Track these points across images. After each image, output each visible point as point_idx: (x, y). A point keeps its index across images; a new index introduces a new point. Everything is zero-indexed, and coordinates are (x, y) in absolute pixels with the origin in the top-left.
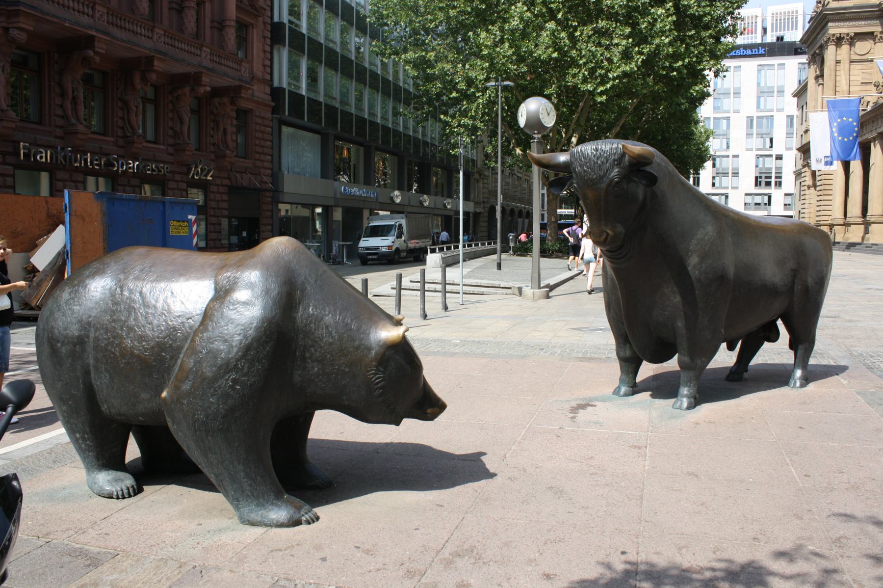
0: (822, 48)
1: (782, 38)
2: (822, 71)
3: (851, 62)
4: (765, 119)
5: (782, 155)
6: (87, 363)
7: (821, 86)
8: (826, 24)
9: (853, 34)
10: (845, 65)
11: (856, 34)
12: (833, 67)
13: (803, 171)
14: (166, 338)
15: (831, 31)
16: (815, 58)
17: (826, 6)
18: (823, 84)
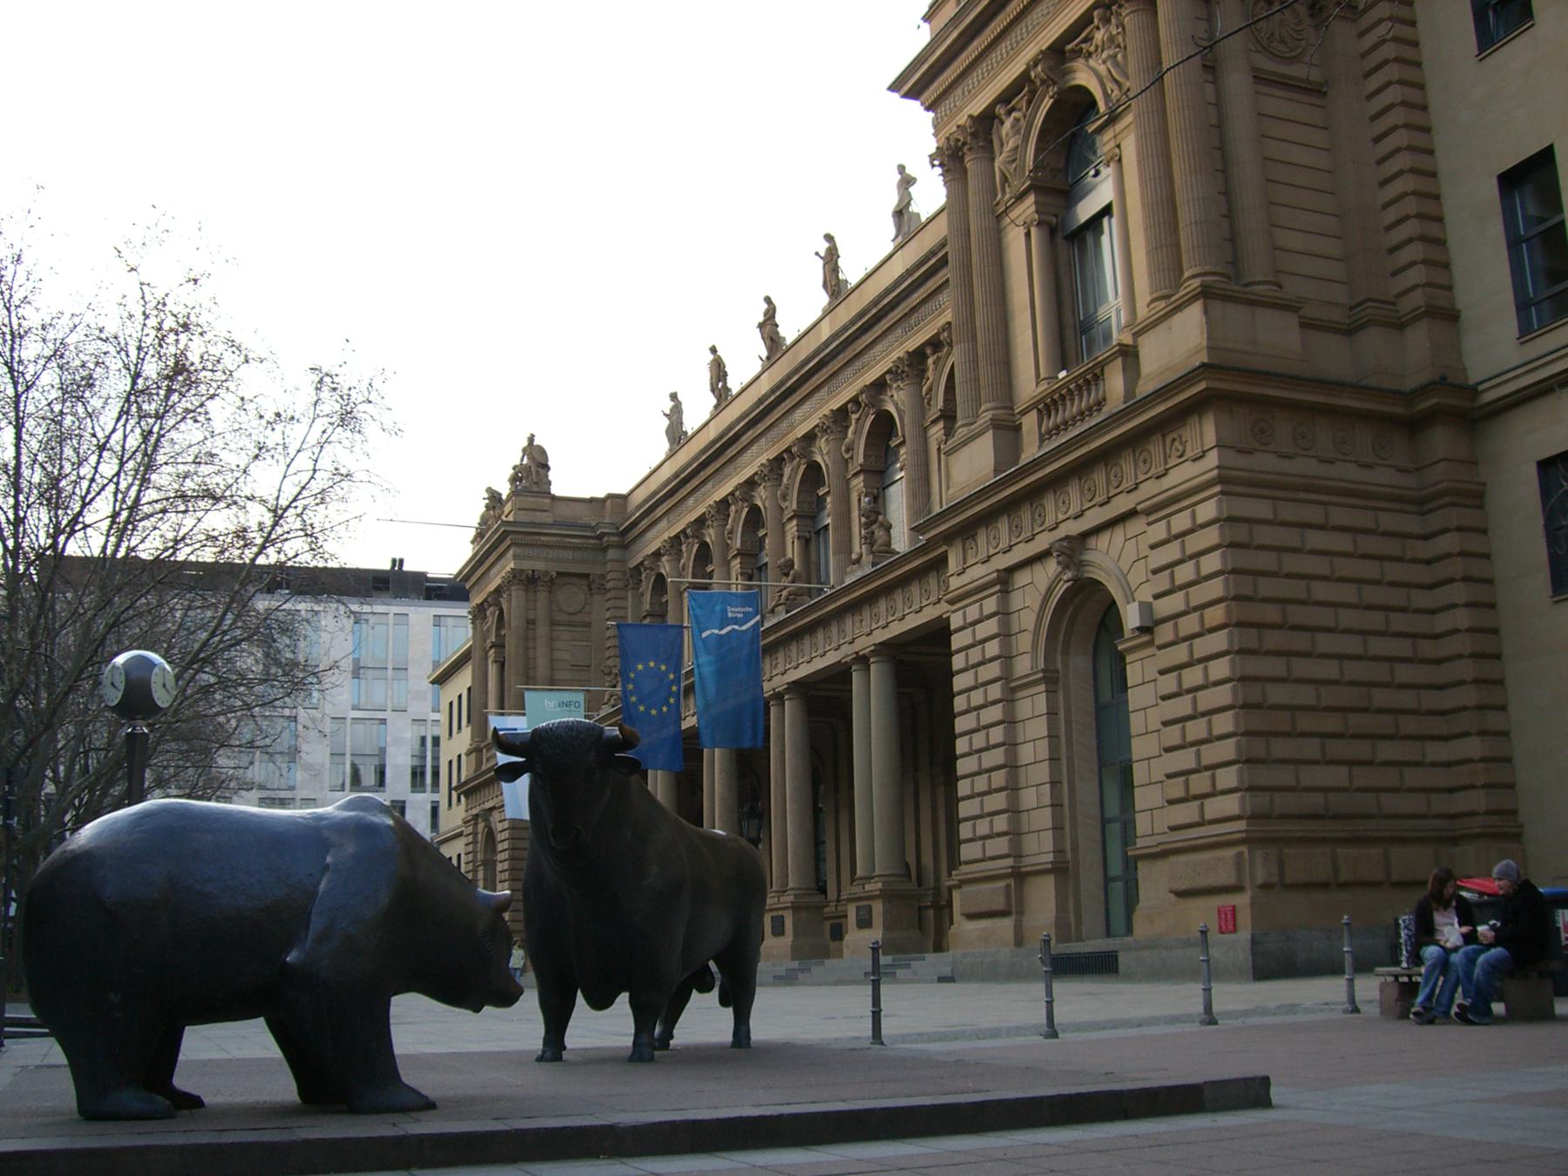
1: (401, 561)
5: (404, 802)
9: (555, 575)
10: (542, 630)
11: (559, 574)
16: (485, 610)
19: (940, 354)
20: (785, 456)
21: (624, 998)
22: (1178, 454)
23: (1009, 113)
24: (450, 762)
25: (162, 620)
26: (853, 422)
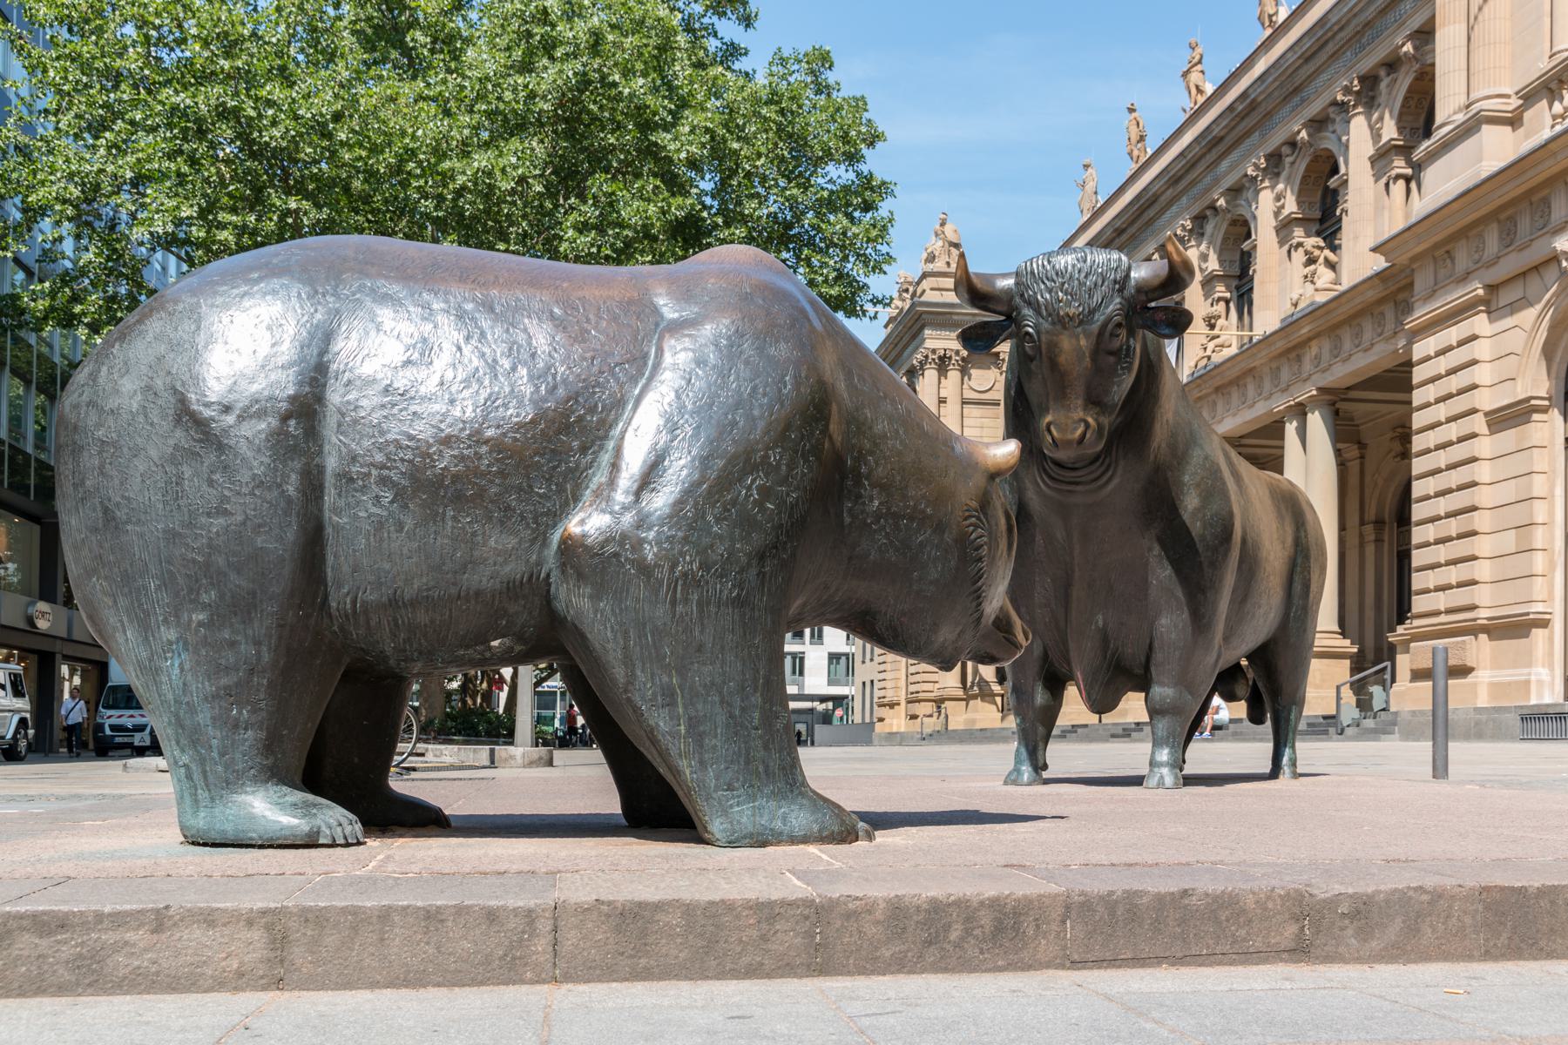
3: (964, 402)
6: (318, 466)
14: (568, 401)
15: (929, 344)
19: (1394, 75)
20: (1208, 213)
26: (1287, 166)
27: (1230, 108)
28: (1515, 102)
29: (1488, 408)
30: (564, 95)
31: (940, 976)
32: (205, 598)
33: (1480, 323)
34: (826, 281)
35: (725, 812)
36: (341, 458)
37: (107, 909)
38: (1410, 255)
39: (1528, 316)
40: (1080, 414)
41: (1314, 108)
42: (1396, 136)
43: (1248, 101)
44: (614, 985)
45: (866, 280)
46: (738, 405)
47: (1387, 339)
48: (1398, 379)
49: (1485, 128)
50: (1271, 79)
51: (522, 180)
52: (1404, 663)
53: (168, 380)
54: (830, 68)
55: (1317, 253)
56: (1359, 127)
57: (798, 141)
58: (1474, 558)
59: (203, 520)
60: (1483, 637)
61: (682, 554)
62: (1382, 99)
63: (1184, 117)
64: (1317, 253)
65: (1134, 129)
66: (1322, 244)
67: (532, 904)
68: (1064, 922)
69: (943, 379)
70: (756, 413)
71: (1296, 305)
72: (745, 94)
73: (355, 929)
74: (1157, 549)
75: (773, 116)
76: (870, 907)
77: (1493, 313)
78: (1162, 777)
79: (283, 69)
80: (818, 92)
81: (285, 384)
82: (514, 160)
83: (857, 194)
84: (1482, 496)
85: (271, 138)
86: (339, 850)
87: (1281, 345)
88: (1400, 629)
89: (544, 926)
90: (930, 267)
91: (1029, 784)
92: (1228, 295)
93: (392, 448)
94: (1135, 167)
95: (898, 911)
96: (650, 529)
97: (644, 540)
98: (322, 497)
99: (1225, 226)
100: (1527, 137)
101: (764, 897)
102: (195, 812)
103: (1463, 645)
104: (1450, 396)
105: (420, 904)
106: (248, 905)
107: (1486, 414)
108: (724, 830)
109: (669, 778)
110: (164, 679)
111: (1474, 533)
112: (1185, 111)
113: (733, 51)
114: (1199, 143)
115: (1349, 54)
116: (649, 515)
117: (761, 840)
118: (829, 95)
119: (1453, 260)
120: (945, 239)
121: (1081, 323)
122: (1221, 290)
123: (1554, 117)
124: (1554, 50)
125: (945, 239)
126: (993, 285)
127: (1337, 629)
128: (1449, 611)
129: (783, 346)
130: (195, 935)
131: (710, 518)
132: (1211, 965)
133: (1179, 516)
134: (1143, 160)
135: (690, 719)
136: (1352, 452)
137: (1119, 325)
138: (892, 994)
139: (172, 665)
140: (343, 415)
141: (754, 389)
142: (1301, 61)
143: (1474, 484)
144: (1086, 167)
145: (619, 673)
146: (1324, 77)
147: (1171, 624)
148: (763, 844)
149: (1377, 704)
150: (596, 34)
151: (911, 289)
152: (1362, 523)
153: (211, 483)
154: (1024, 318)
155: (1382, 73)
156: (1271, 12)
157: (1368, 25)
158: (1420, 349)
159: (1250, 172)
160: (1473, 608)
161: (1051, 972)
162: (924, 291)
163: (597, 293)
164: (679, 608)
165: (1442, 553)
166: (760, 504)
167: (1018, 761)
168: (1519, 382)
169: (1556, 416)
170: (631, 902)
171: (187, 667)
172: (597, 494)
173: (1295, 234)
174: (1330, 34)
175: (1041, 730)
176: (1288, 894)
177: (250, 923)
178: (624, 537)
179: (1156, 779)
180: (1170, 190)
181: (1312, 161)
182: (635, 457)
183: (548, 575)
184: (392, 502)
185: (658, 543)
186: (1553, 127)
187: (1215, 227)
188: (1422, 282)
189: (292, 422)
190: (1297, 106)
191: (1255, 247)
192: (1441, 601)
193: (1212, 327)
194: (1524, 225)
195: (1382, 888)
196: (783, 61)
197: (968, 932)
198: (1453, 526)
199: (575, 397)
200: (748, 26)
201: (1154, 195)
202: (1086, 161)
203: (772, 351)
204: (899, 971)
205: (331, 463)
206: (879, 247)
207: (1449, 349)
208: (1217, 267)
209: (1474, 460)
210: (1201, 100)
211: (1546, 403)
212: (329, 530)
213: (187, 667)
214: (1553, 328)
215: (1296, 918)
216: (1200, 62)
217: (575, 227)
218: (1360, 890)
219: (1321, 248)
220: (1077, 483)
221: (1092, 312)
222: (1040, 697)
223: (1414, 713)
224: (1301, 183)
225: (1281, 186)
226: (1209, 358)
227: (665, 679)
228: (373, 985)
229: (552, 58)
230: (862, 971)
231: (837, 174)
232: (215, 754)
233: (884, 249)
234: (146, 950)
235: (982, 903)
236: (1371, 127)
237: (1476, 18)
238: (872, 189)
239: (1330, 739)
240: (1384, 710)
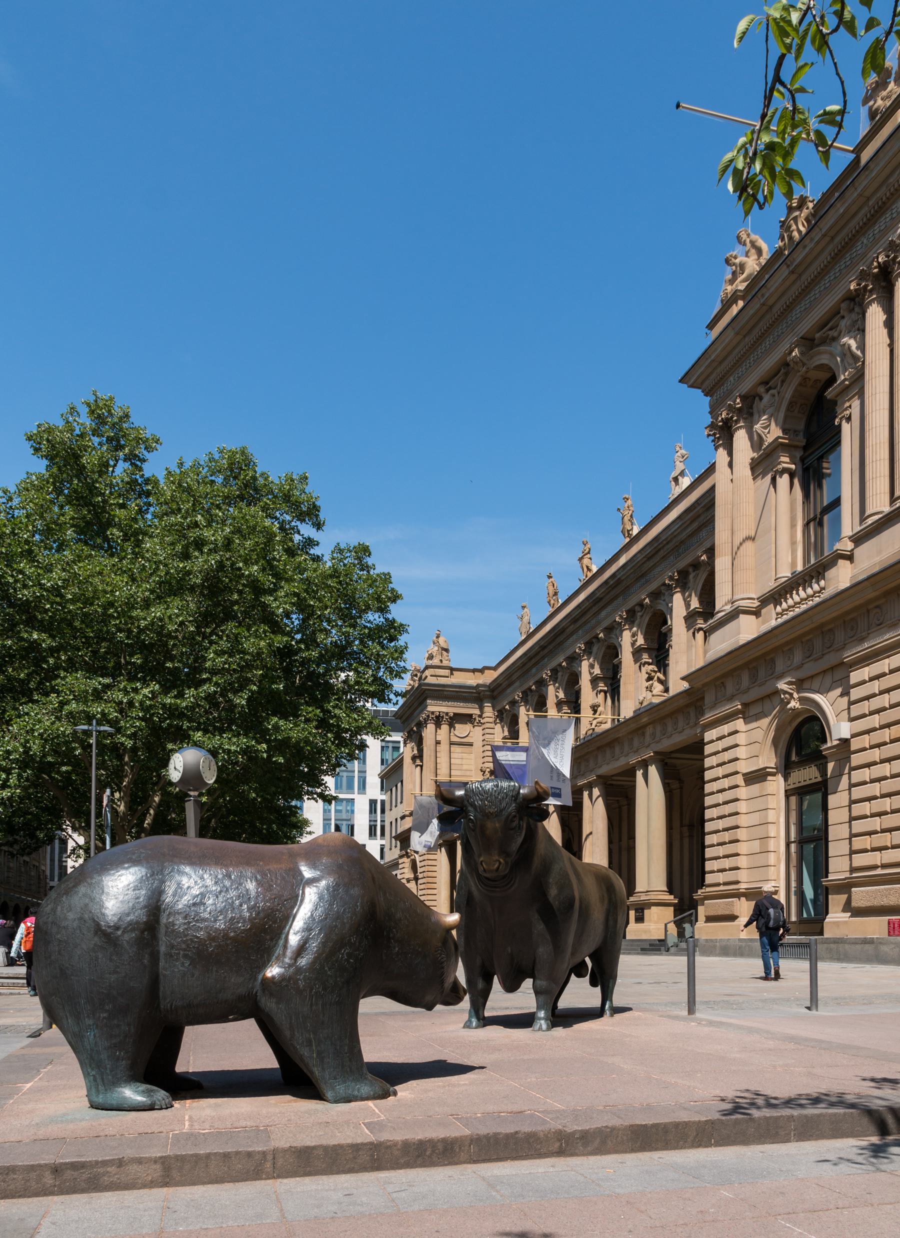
0: (421, 725)
2: (421, 750)
3: (452, 744)
4: (345, 802)
7: (419, 767)
8: (425, 699)
10: (444, 748)
11: (455, 714)
12: (433, 748)
13: (401, 861)
15: (430, 708)
17: (424, 679)
18: (422, 766)
19: (698, 572)
20: (594, 640)
21: (528, 983)
22: (878, 622)
23: (767, 391)
24: (391, 823)
25: (236, 751)
27: (606, 582)
28: (756, 603)
29: (745, 771)
30: (208, 574)
31: (423, 1169)
32: (107, 1007)
33: (739, 724)
34: (366, 682)
35: (333, 1089)
36: (167, 946)
37: (100, 1159)
38: (702, 683)
39: (765, 722)
40: (497, 858)
41: (653, 586)
42: (698, 606)
43: (616, 579)
44: (297, 1179)
45: (392, 682)
46: (337, 918)
47: (692, 727)
48: (697, 747)
49: (741, 616)
50: (629, 568)
51: (182, 623)
52: (701, 910)
53: (91, 915)
54: (369, 556)
55: (653, 674)
56: (678, 600)
57: (351, 601)
58: (737, 855)
59: (107, 976)
60: (743, 899)
61: (315, 985)
62: (691, 584)
63: (579, 584)
64: (653, 674)
65: (551, 588)
66: (656, 669)
67: (265, 1149)
68: (470, 1146)
69: (438, 730)
70: (345, 921)
71: (641, 703)
72: (318, 573)
73: (196, 1162)
74: (536, 916)
75: (335, 585)
76: (395, 1144)
77: (747, 720)
78: (541, 1025)
79: (30, 552)
80: (362, 570)
81: (140, 915)
82: (176, 611)
83: (386, 632)
84: (742, 820)
85: (23, 595)
86: (164, 1110)
87: (633, 726)
88: (700, 892)
89: (270, 1157)
90: (430, 662)
91: (476, 1028)
92: (606, 688)
93: (189, 942)
94: (552, 610)
95: (406, 1145)
96: (301, 974)
97: (299, 979)
98: (158, 964)
99: (603, 649)
100: (763, 623)
101: (355, 1142)
102: (97, 1096)
103: (732, 904)
104: (724, 763)
105: (221, 1151)
106: (154, 1155)
107: (744, 775)
108: (333, 1096)
109: (309, 1074)
110: (86, 1040)
111: (737, 841)
112: (580, 580)
113: (310, 543)
114: (589, 601)
115: (672, 557)
116: (301, 968)
117: (348, 1100)
118: (368, 572)
119: (725, 687)
120: (439, 646)
121: (496, 816)
122: (602, 686)
123: (778, 614)
124: (778, 576)
125: (439, 646)
126: (454, 794)
127: (665, 889)
128: (725, 884)
129: (356, 889)
130: (134, 1168)
131: (326, 968)
132: (526, 1159)
133: (548, 899)
134: (556, 606)
135: (318, 1051)
136: (675, 785)
137: (515, 816)
138: (404, 1180)
139: (90, 1034)
140: (168, 928)
141: (344, 910)
142: (645, 559)
143: (737, 813)
144: (523, 607)
145: (288, 1033)
146: (659, 569)
147: (543, 951)
148: (350, 1101)
149: (688, 934)
150: (228, 539)
151: (419, 675)
152: (682, 826)
153: (111, 960)
154: (469, 811)
155: (691, 570)
156: (629, 529)
157: (682, 542)
158: (709, 735)
159: (617, 619)
160: (737, 882)
161: (465, 1165)
162: (426, 677)
163: (275, 867)
164: (314, 1008)
165: (721, 851)
166: (347, 960)
167: (470, 1016)
168: (761, 758)
169: (780, 778)
170: (304, 1147)
171: (97, 1035)
172: (278, 958)
173: (644, 657)
174: (661, 546)
175: (481, 1000)
176: (556, 1131)
177: (155, 1162)
178: (290, 978)
179: (538, 1026)
180: (572, 626)
181: (652, 616)
182: (294, 940)
183: (256, 993)
184: (189, 965)
185: (305, 981)
186: (776, 619)
187: (598, 649)
188: (709, 699)
189: (146, 933)
190: (644, 584)
191: (621, 662)
192: (721, 878)
193: (595, 712)
194: (762, 673)
195: (592, 1127)
196: (341, 551)
197: (433, 1151)
198: (726, 836)
199: (267, 916)
200: (318, 529)
201: (563, 628)
202: (524, 604)
203: (352, 892)
204: (407, 1168)
205: (163, 949)
206: (399, 663)
207: (723, 737)
208: (599, 672)
209: (737, 800)
210: (590, 575)
211: (775, 770)
212: (161, 977)
213: (97, 1035)
214: (777, 730)
215: (559, 1140)
216: (589, 553)
217: (215, 652)
218: (583, 1128)
219: (655, 672)
220: (496, 887)
221: (501, 811)
222: (480, 985)
223: (706, 940)
224: (646, 628)
225: (635, 629)
226: (593, 729)
227: (307, 1035)
228: (204, 1183)
229: (202, 553)
230: (393, 1168)
231: (374, 618)
232: (108, 1071)
233: (402, 664)
234: (115, 1174)
235: (438, 1140)
236: (685, 600)
237: (736, 553)
238: (395, 628)
239: (661, 954)
240: (691, 937)
